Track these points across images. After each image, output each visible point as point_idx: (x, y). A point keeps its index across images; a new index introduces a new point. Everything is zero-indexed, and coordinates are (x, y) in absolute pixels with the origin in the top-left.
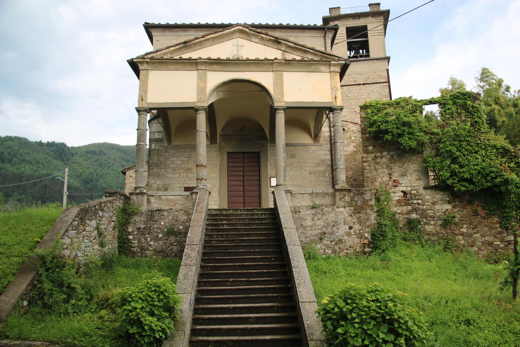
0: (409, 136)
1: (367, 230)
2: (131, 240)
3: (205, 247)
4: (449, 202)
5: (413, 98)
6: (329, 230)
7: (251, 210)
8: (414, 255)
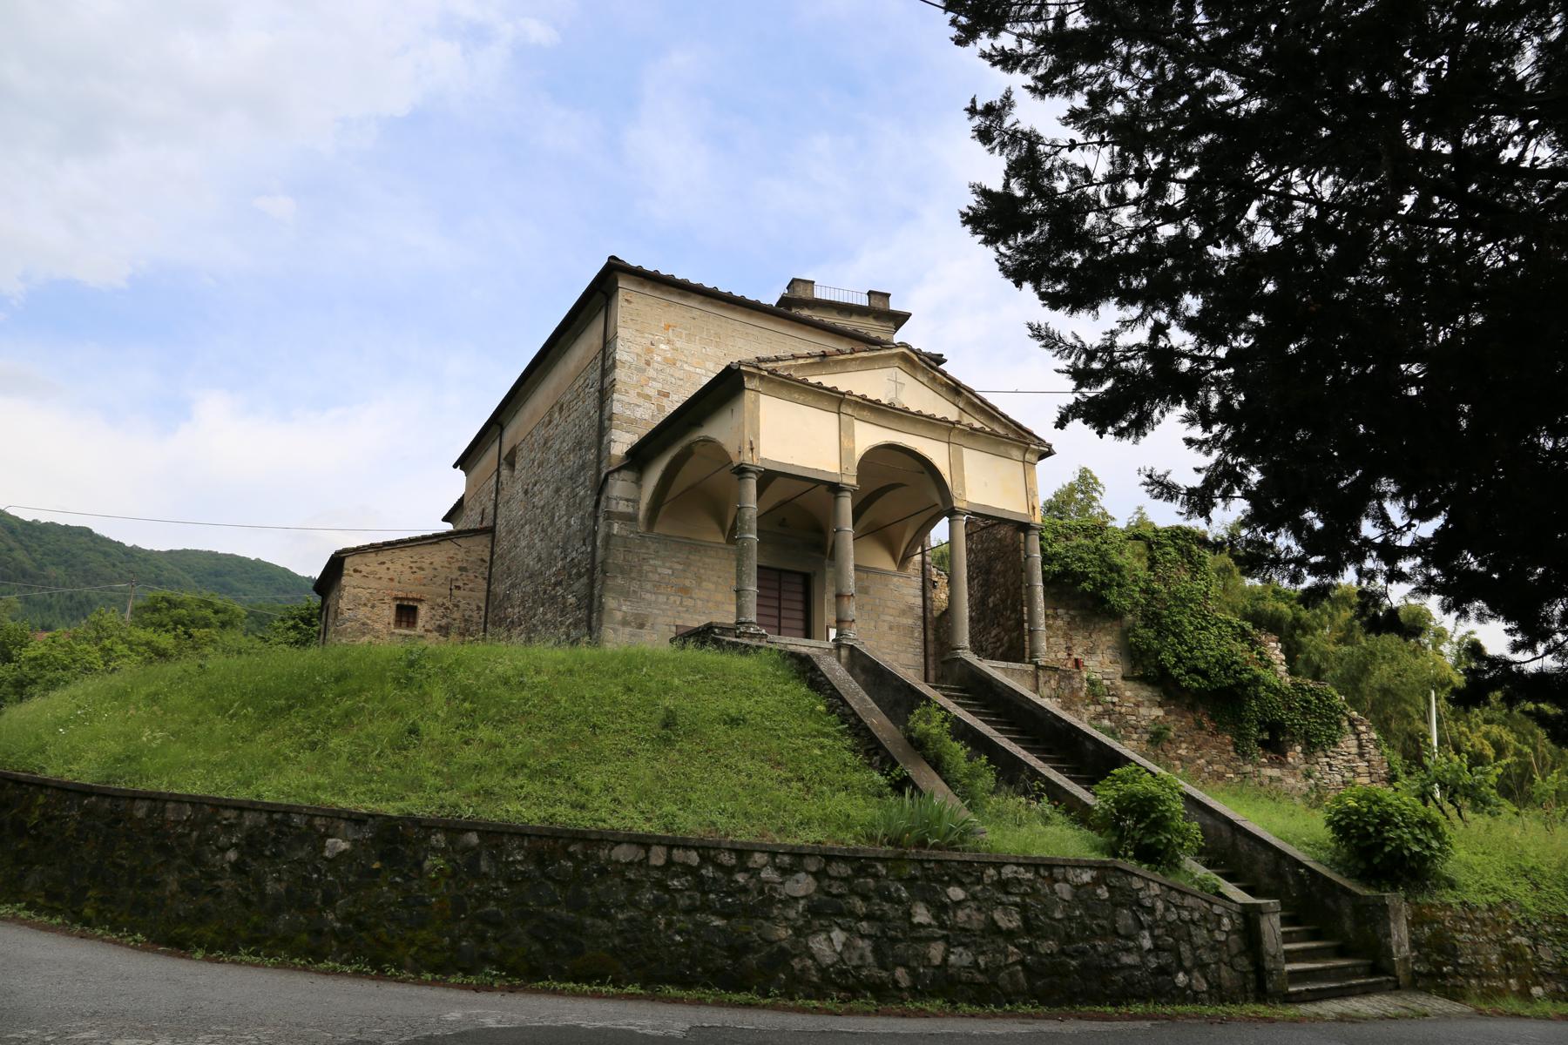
4: (1160, 705)
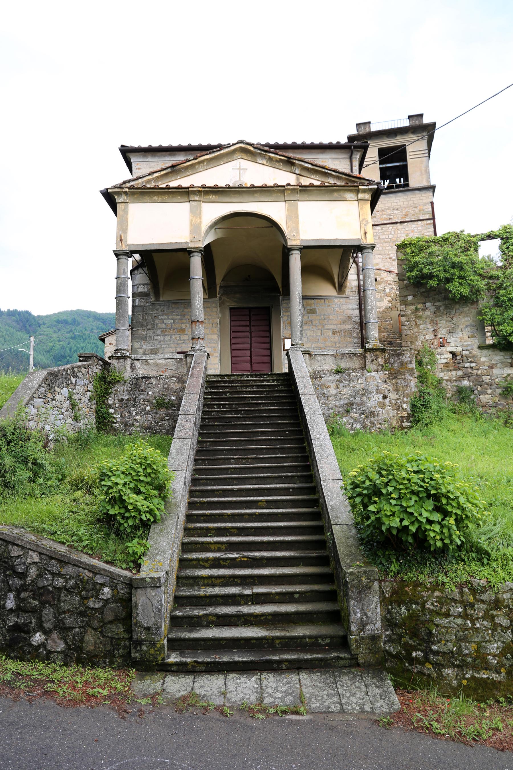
0: (460, 281)
1: (405, 399)
2: (112, 414)
3: (203, 419)
5: (466, 233)
6: (358, 400)
7: (260, 376)
8: (465, 430)
